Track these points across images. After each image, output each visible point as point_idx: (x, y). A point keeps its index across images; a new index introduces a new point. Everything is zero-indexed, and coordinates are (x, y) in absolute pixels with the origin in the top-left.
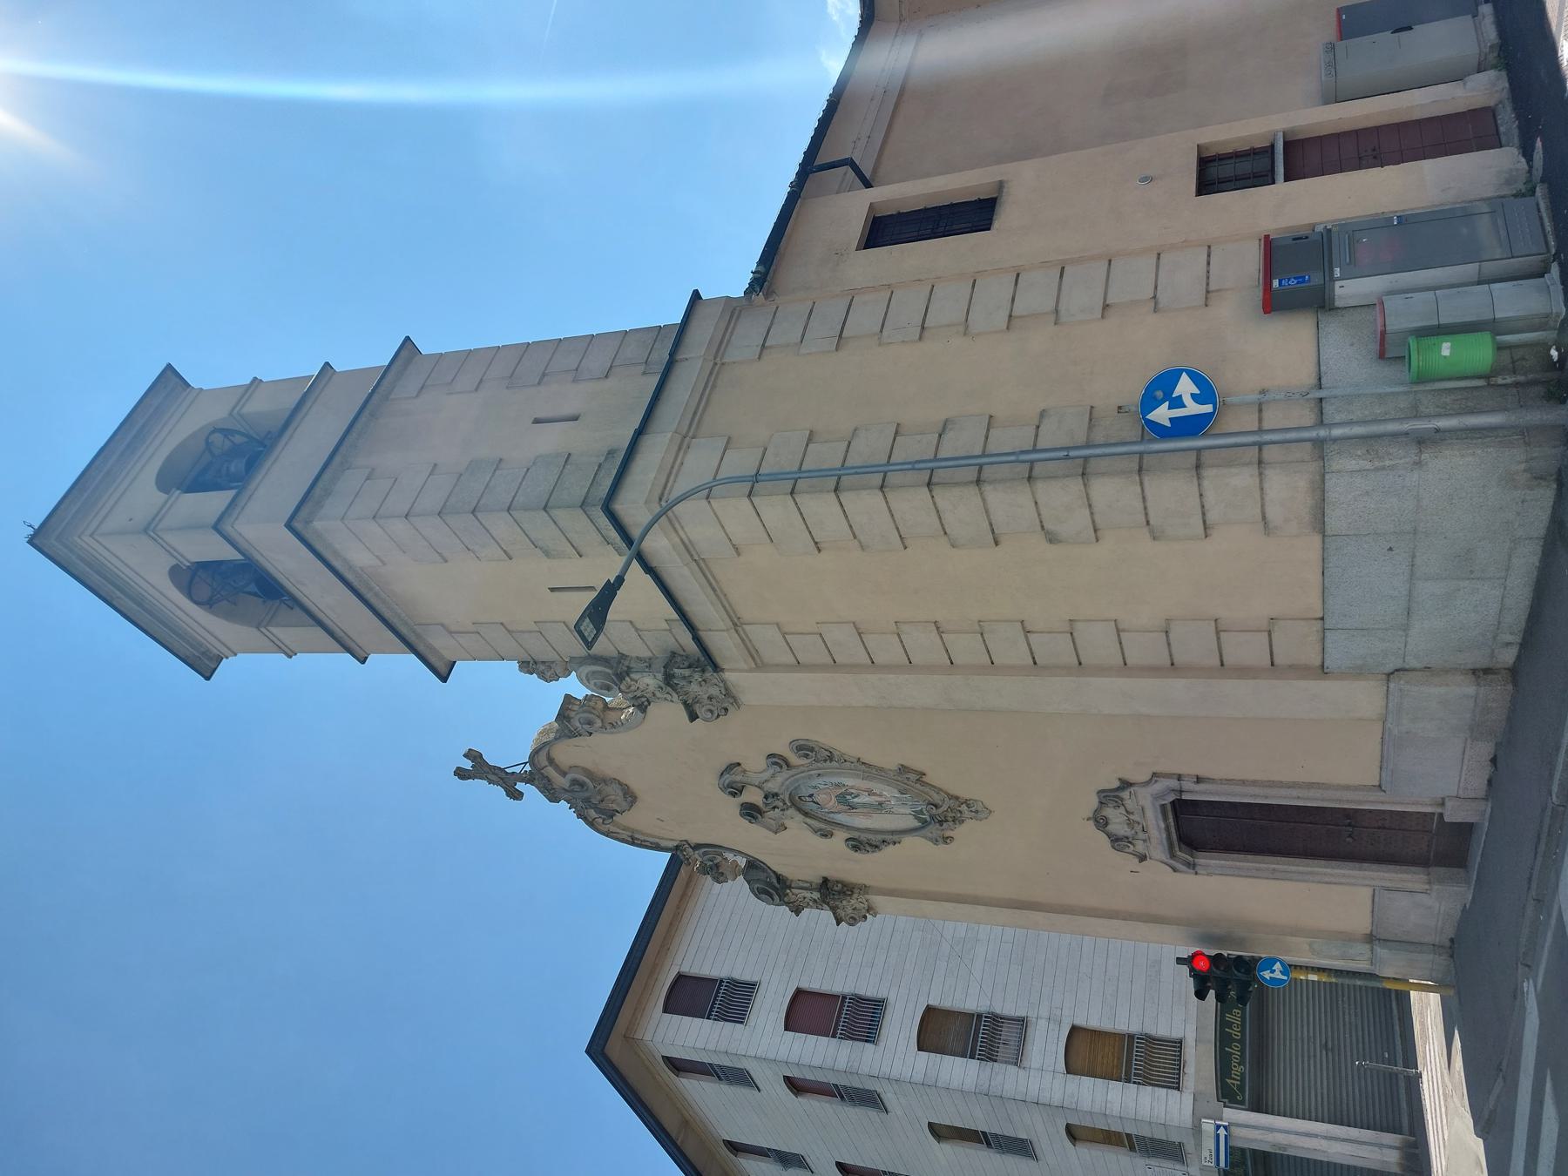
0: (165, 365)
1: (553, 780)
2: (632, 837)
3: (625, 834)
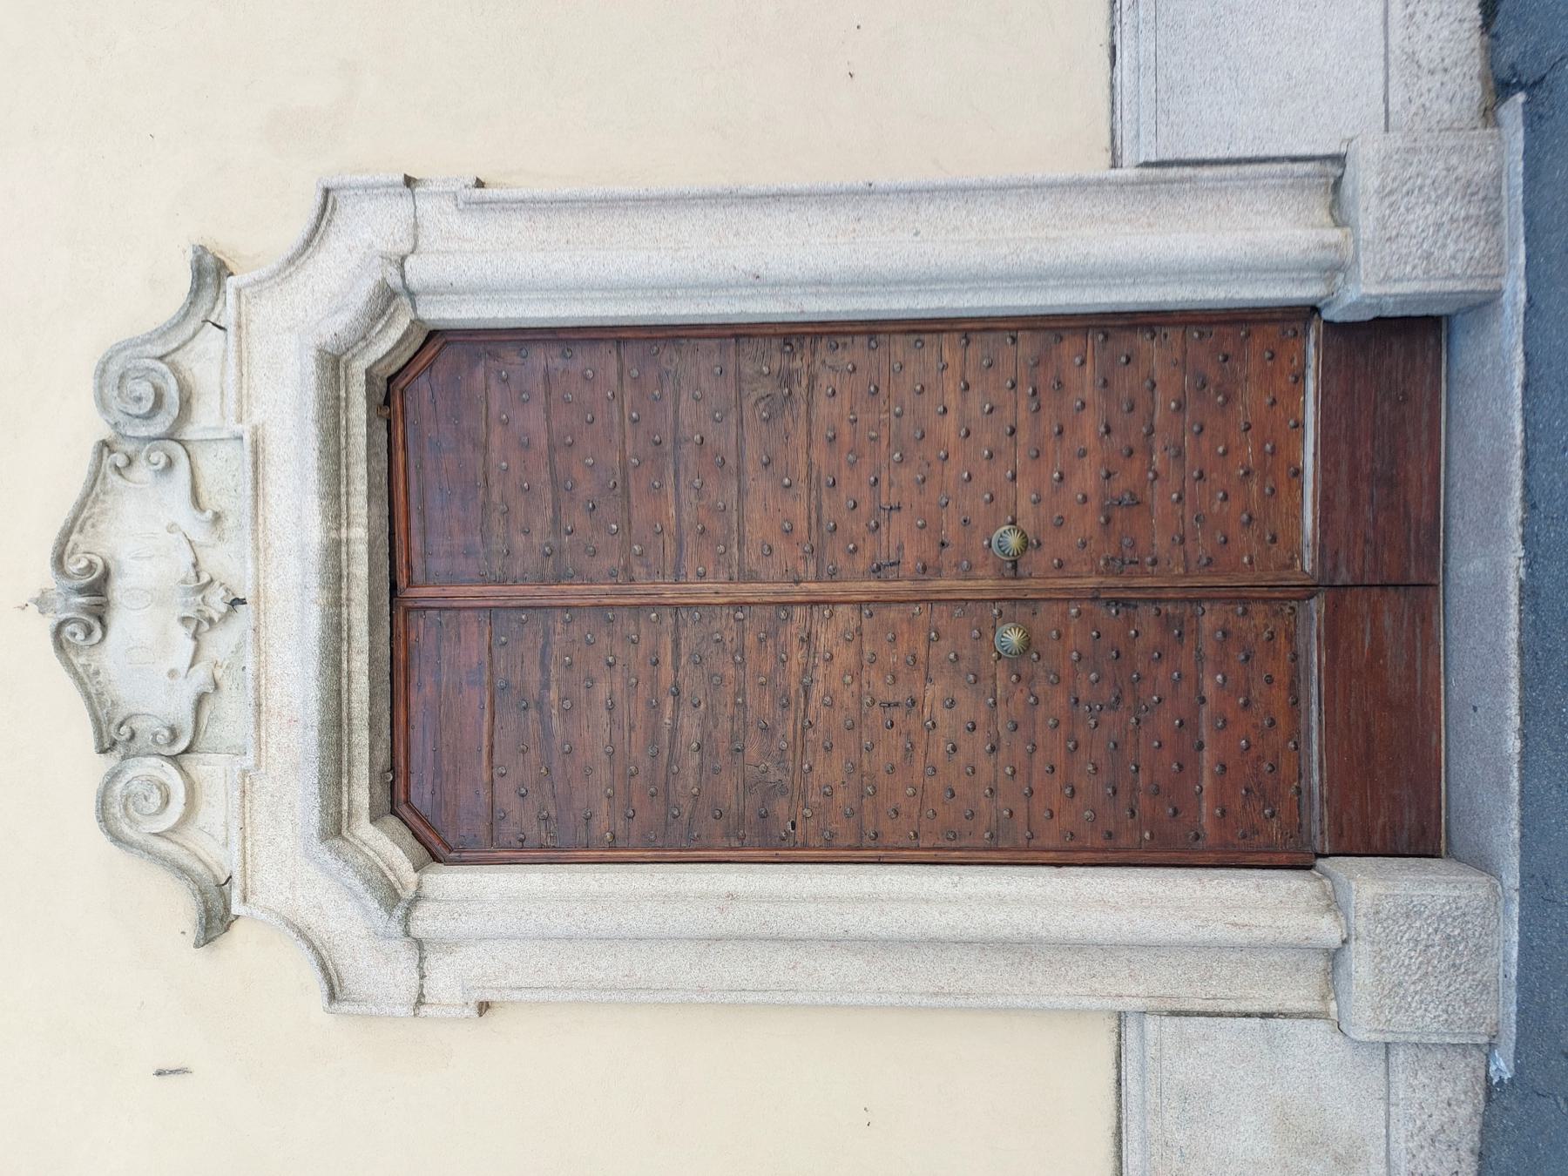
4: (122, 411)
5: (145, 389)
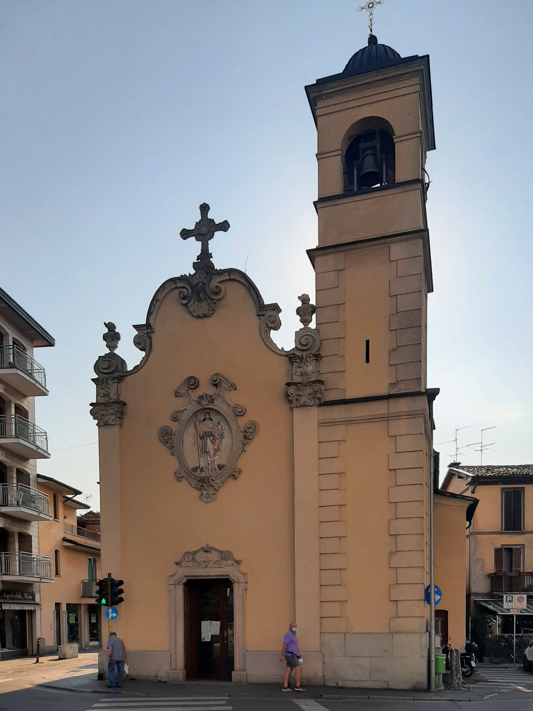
0: (281, 308)
1: (218, 276)
2: (158, 300)
3: (160, 297)
4: (8, 709)
5: (227, 556)
